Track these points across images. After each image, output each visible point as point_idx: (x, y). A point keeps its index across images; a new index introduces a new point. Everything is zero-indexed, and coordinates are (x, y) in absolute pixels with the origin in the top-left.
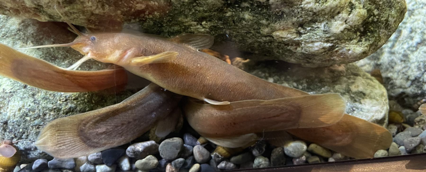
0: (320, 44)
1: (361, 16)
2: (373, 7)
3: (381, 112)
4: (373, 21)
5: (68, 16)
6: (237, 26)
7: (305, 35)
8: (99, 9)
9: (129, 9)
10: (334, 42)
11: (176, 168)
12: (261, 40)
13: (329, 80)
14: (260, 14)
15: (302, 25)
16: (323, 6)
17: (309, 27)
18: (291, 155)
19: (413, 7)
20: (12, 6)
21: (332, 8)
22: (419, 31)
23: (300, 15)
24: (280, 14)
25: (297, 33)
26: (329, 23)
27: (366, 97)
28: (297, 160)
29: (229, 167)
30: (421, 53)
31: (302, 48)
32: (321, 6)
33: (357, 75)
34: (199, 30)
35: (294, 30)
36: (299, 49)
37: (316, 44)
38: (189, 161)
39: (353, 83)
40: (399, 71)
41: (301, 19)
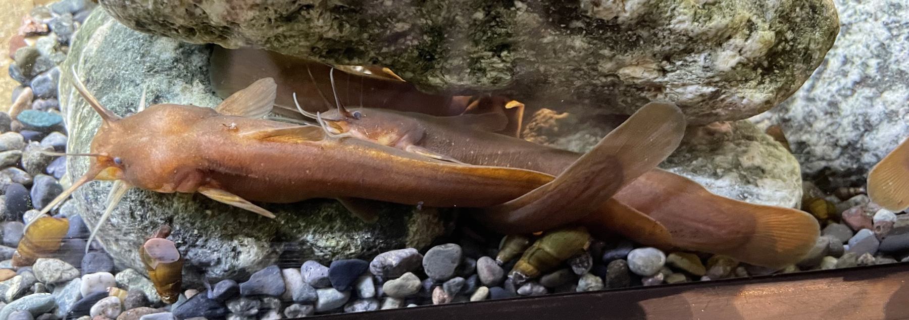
1: (765, 43)
2: (785, 27)
3: (790, 201)
5: (279, 41)
6: (559, 58)
8: (335, 30)
10: (720, 84)
11: (450, 293)
12: (598, 82)
13: (704, 147)
14: (600, 39)
15: (668, 58)
18: (639, 272)
19: (849, 20)
20: (186, 24)
21: (719, 30)
22: (858, 61)
23: (667, 40)
25: (659, 71)
26: (713, 53)
27: (766, 175)
28: (650, 280)
29: (536, 292)
30: (860, 99)
31: (666, 95)
33: (750, 138)
35: (654, 66)
36: (660, 96)
38: (472, 282)
39: (745, 152)
40: (822, 131)
41: (668, 48)
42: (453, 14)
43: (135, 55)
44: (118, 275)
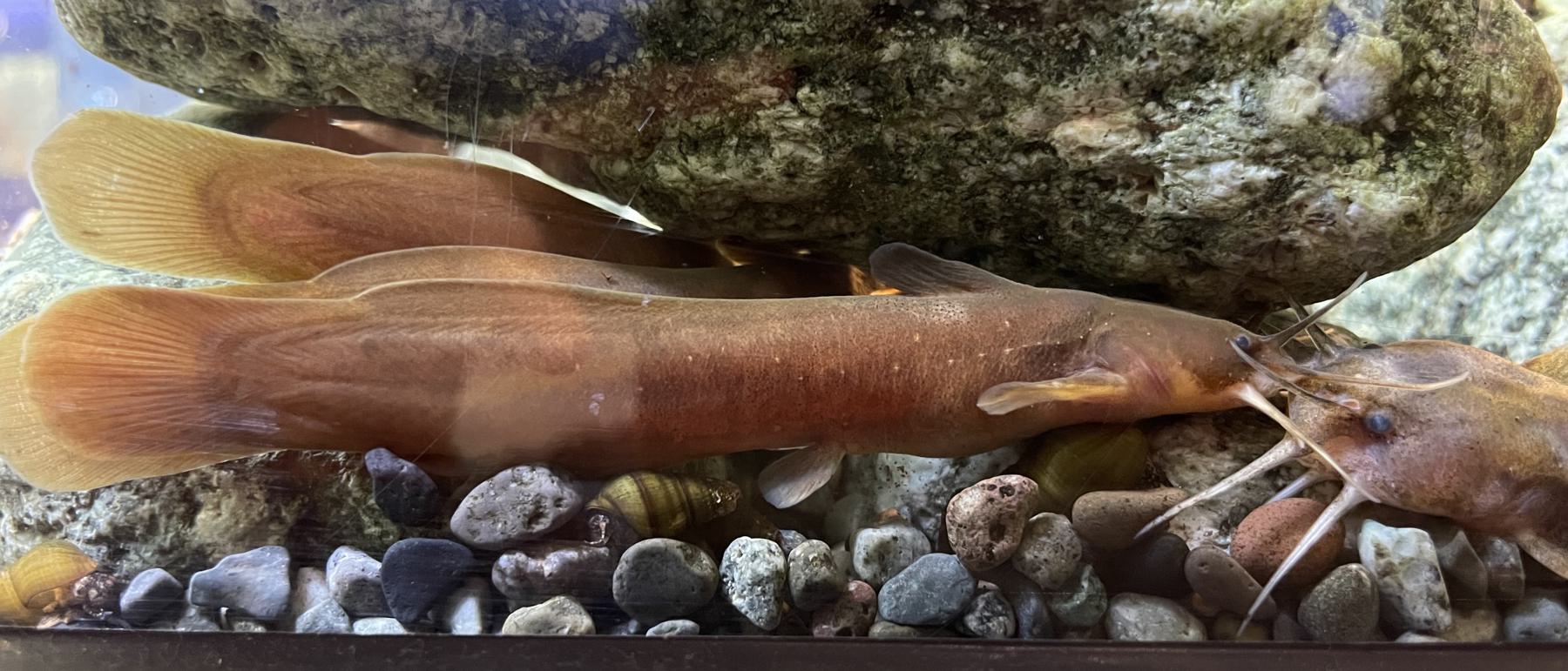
4: (1428, 91)
6: (919, 104)
7: (1173, 133)
9: (552, 33)
10: (1286, 160)
12: (1012, 168)
14: (1001, 45)
15: (1157, 91)
16: (1228, 14)
17: (1185, 100)
21: (1264, 24)
24: (1076, 45)
26: (1258, 81)
32: (1225, 11)
34: (786, 123)
35: (1129, 116)
36: (1154, 200)
37: (1218, 170)
41: (1153, 65)
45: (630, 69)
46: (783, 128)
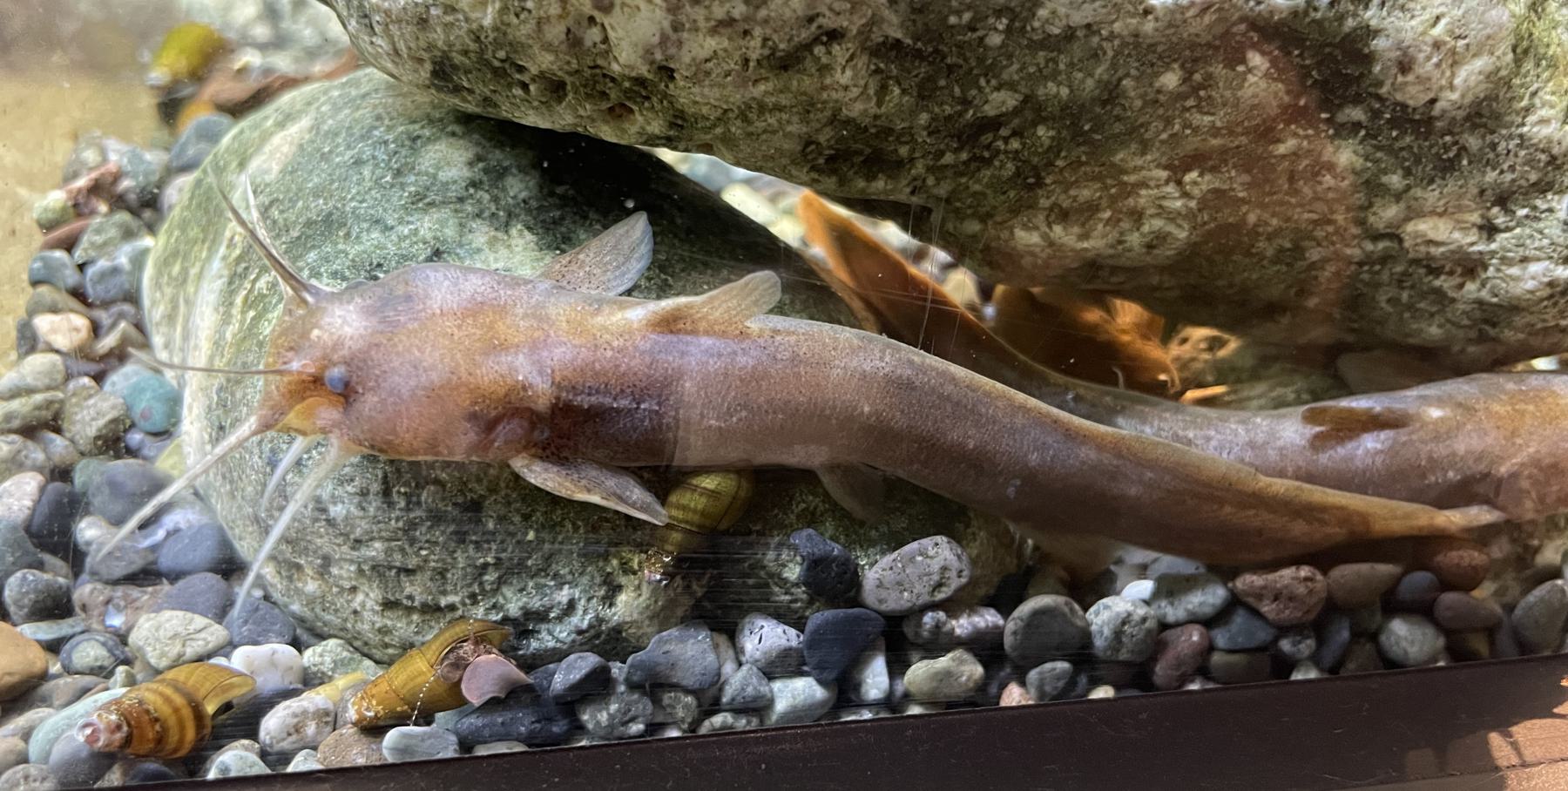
0: (1548, 269)
6: (1296, 192)
7: (1507, 235)
14: (1390, 150)
15: (1504, 200)
25: (1481, 228)
34: (1166, 203)
36: (1471, 287)
37: (1534, 268)
41: (1508, 177)
42: (1120, 73)
43: (378, 172)
44: (308, 653)
45: (1024, 145)
46: (1160, 206)
